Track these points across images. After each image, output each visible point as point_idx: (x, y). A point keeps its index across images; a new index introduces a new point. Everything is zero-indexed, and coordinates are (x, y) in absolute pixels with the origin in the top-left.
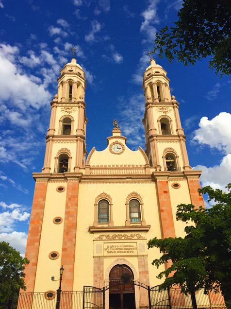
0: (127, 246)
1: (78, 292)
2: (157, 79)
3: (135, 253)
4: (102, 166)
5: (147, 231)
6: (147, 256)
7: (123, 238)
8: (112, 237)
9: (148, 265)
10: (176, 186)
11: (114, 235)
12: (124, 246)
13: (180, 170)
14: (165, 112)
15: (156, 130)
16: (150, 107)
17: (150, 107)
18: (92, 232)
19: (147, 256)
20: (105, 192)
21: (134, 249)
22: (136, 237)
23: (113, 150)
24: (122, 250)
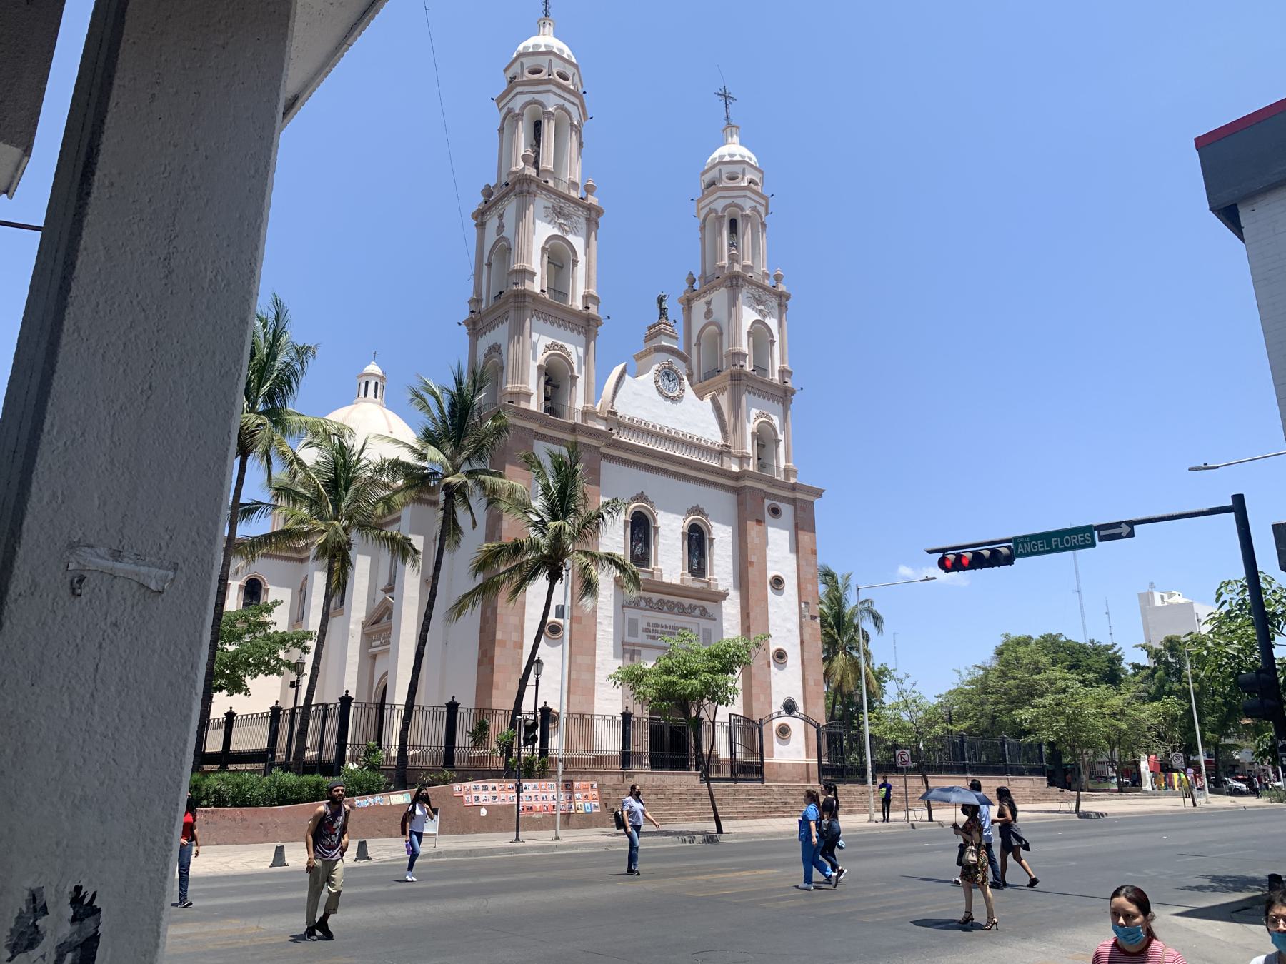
11: (660, 600)
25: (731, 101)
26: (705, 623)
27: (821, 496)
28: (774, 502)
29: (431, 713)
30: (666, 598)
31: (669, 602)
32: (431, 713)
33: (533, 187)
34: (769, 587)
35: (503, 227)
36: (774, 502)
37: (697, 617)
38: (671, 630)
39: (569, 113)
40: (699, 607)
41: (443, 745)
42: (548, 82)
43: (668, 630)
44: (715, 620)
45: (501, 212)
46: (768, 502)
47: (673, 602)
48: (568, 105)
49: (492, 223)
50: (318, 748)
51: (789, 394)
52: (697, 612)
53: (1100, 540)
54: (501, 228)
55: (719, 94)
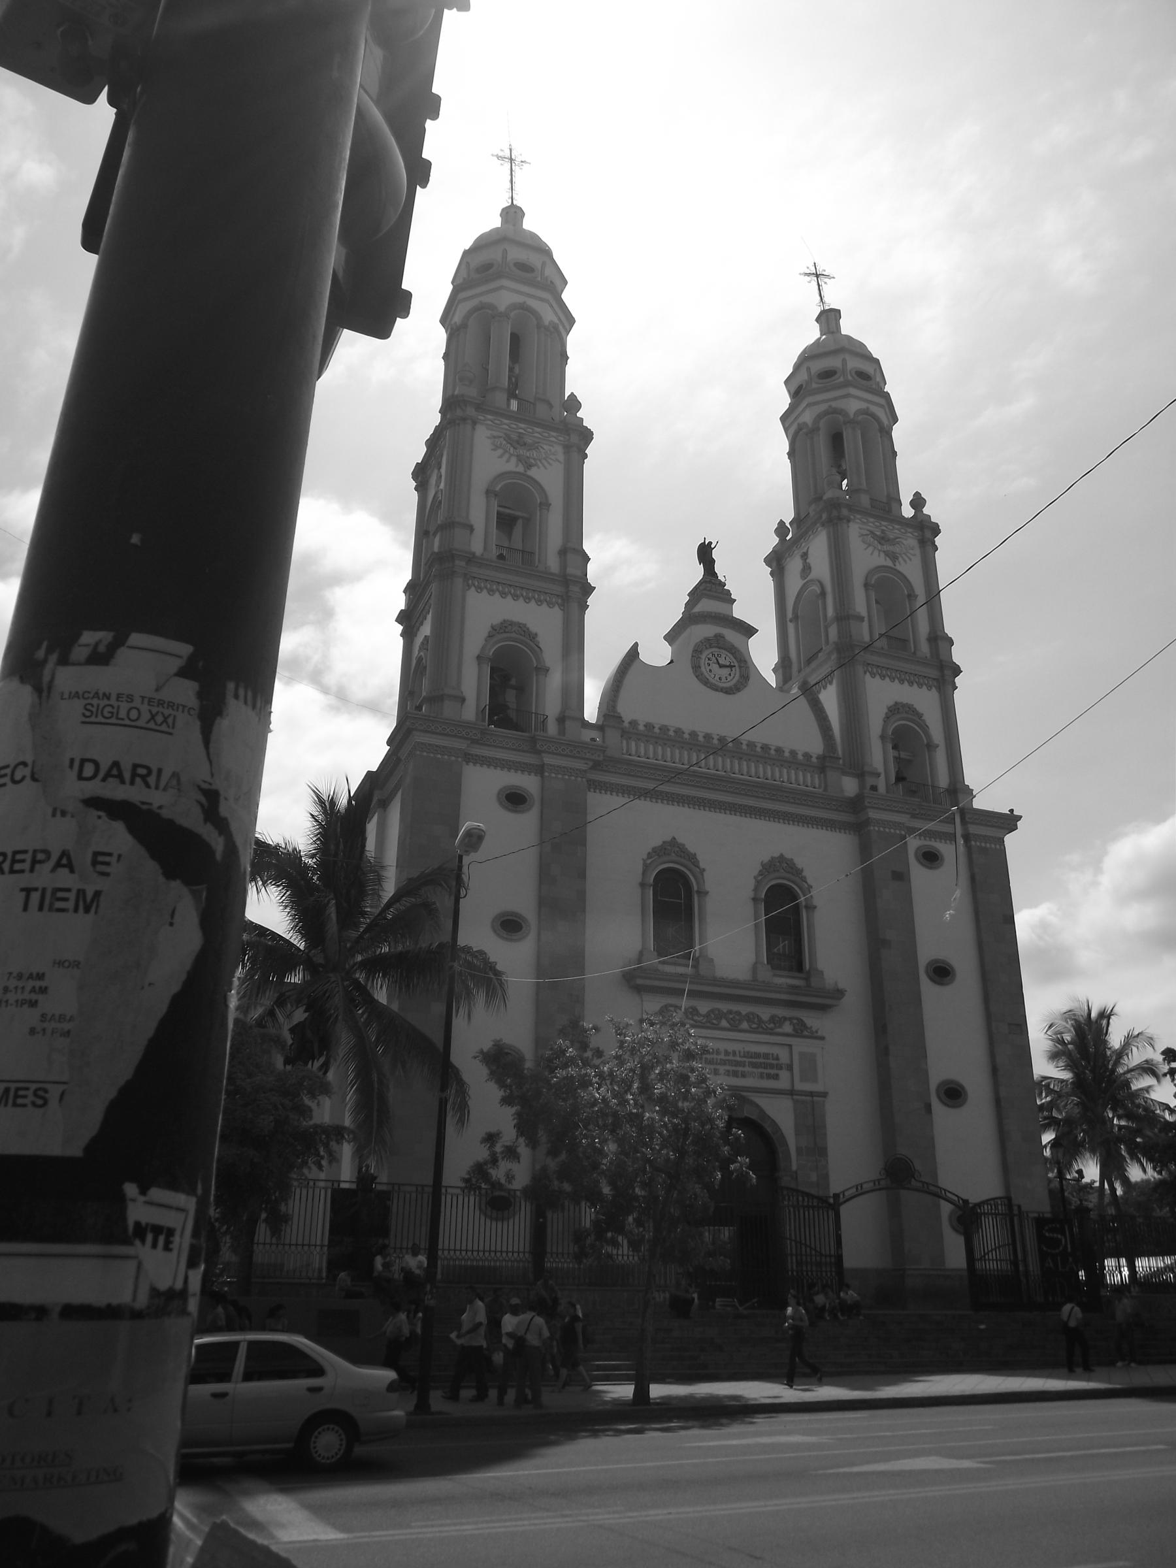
0: (757, 1055)
1: (449, 1190)
2: (518, 299)
3: (783, 1083)
4: (664, 729)
5: (823, 1008)
6: (824, 1095)
7: (745, 1025)
8: (707, 1015)
9: (825, 1127)
10: (931, 858)
11: (712, 1011)
12: (748, 1055)
13: (544, 729)
14: (894, 557)
15: (471, 528)
16: (464, 419)
17: (464, 419)
18: (639, 990)
19: (824, 1095)
20: (680, 840)
21: (780, 1067)
22: (787, 1028)
23: (703, 661)
24: (740, 1069)
25: (826, 280)
26: (801, 1046)
27: (1014, 828)
28: (928, 843)
29: (461, 1198)
30: (724, 1006)
31: (730, 1012)
32: (461, 1198)
33: (845, 512)
34: (923, 978)
35: (810, 568)
36: (928, 843)
37: (787, 1035)
38: (738, 1059)
39: (873, 416)
40: (790, 1019)
41: (527, 1249)
42: (846, 384)
43: (731, 1058)
44: (822, 1038)
45: (805, 551)
46: (914, 843)
47: (738, 1013)
48: (874, 409)
49: (794, 565)
50: (424, 1244)
51: (948, 672)
52: (787, 1028)
53: (564, 735)
54: (806, 569)
55: (806, 274)
